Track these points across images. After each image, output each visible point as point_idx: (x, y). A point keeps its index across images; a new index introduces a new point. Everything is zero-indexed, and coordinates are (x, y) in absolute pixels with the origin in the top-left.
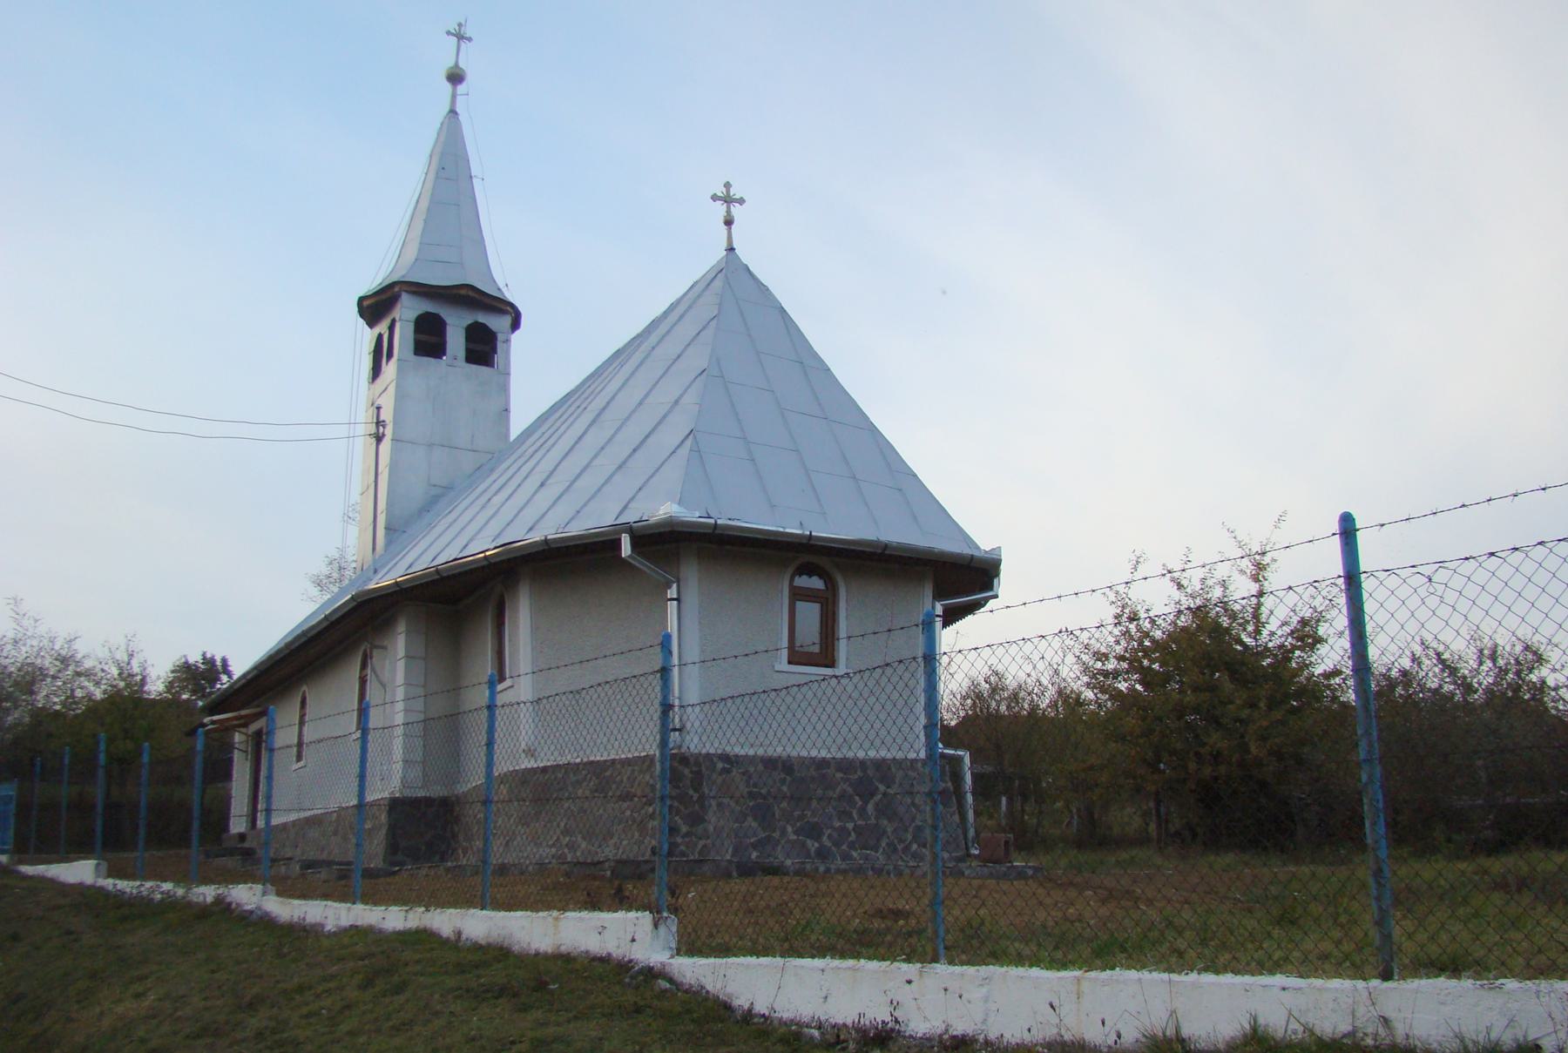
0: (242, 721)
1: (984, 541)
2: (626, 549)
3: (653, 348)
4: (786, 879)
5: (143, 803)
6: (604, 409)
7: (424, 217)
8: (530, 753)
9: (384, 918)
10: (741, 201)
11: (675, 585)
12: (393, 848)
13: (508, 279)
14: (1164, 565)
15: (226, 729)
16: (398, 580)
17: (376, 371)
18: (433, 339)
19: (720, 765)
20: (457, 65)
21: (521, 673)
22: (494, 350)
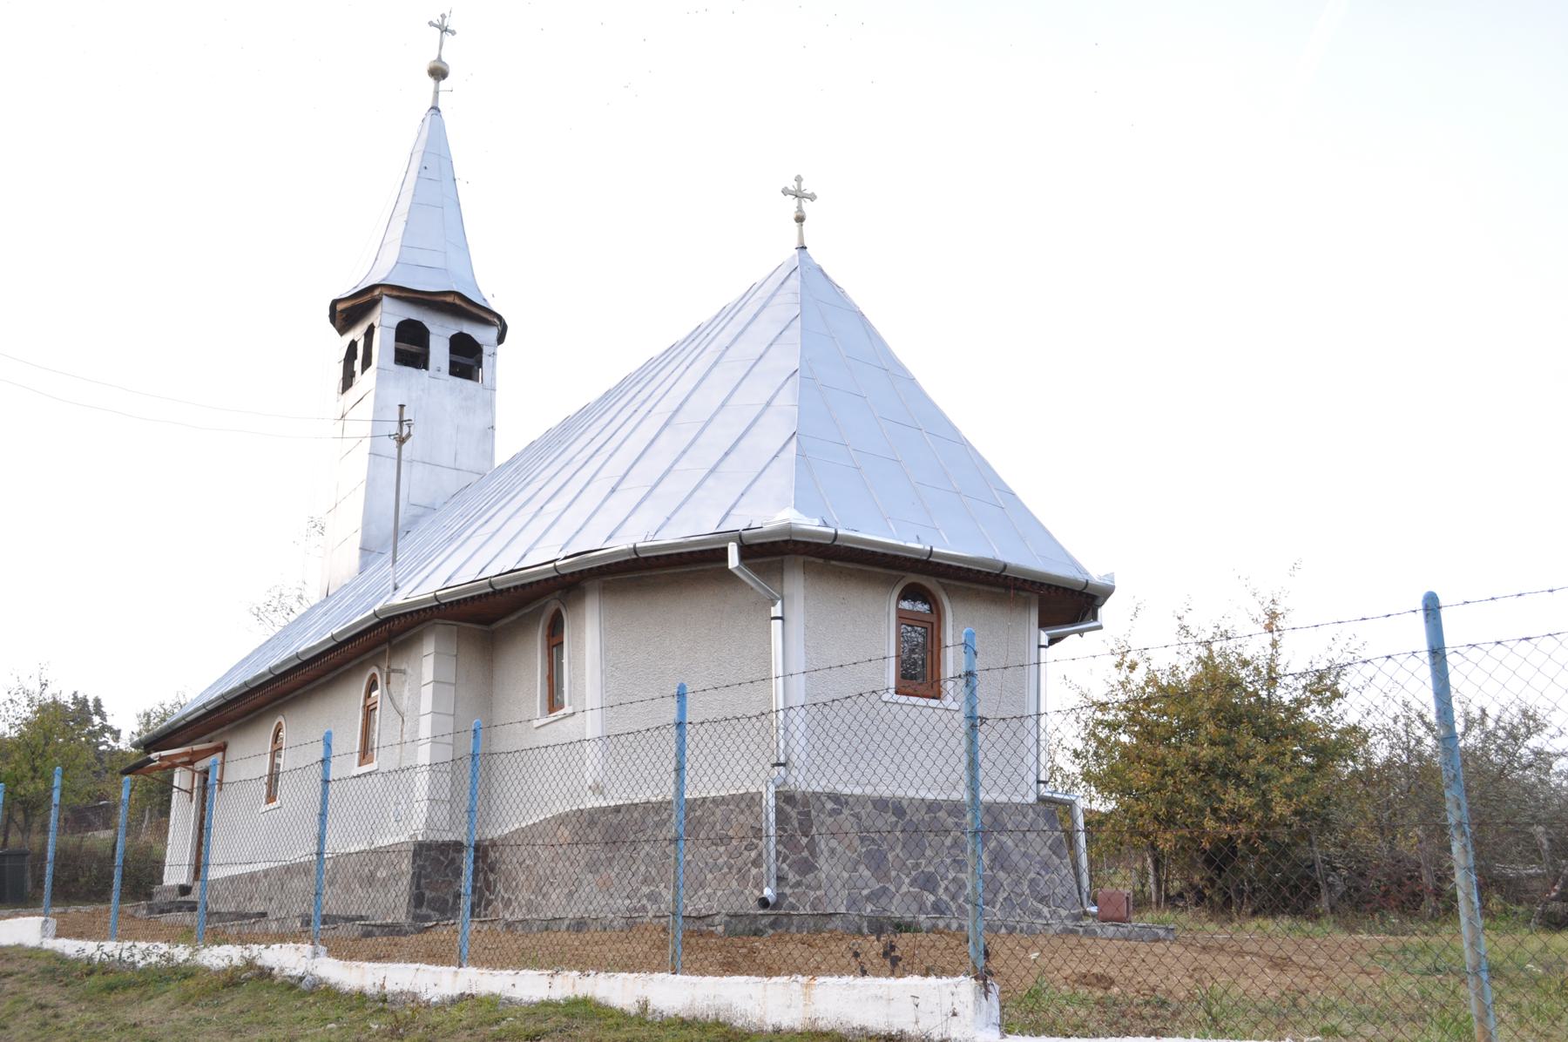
0: (186, 759)
1: (1095, 571)
2: (733, 560)
3: (727, 348)
4: (920, 937)
5: (50, 855)
6: (677, 411)
7: (405, 218)
8: (598, 789)
9: (514, 985)
10: (812, 197)
11: (779, 603)
12: (418, 900)
13: (491, 292)
14: (1174, 612)
15: (170, 767)
16: (438, 593)
17: (348, 381)
18: (414, 349)
19: (830, 805)
20: (439, 57)
21: (803, 677)
22: (480, 364)
